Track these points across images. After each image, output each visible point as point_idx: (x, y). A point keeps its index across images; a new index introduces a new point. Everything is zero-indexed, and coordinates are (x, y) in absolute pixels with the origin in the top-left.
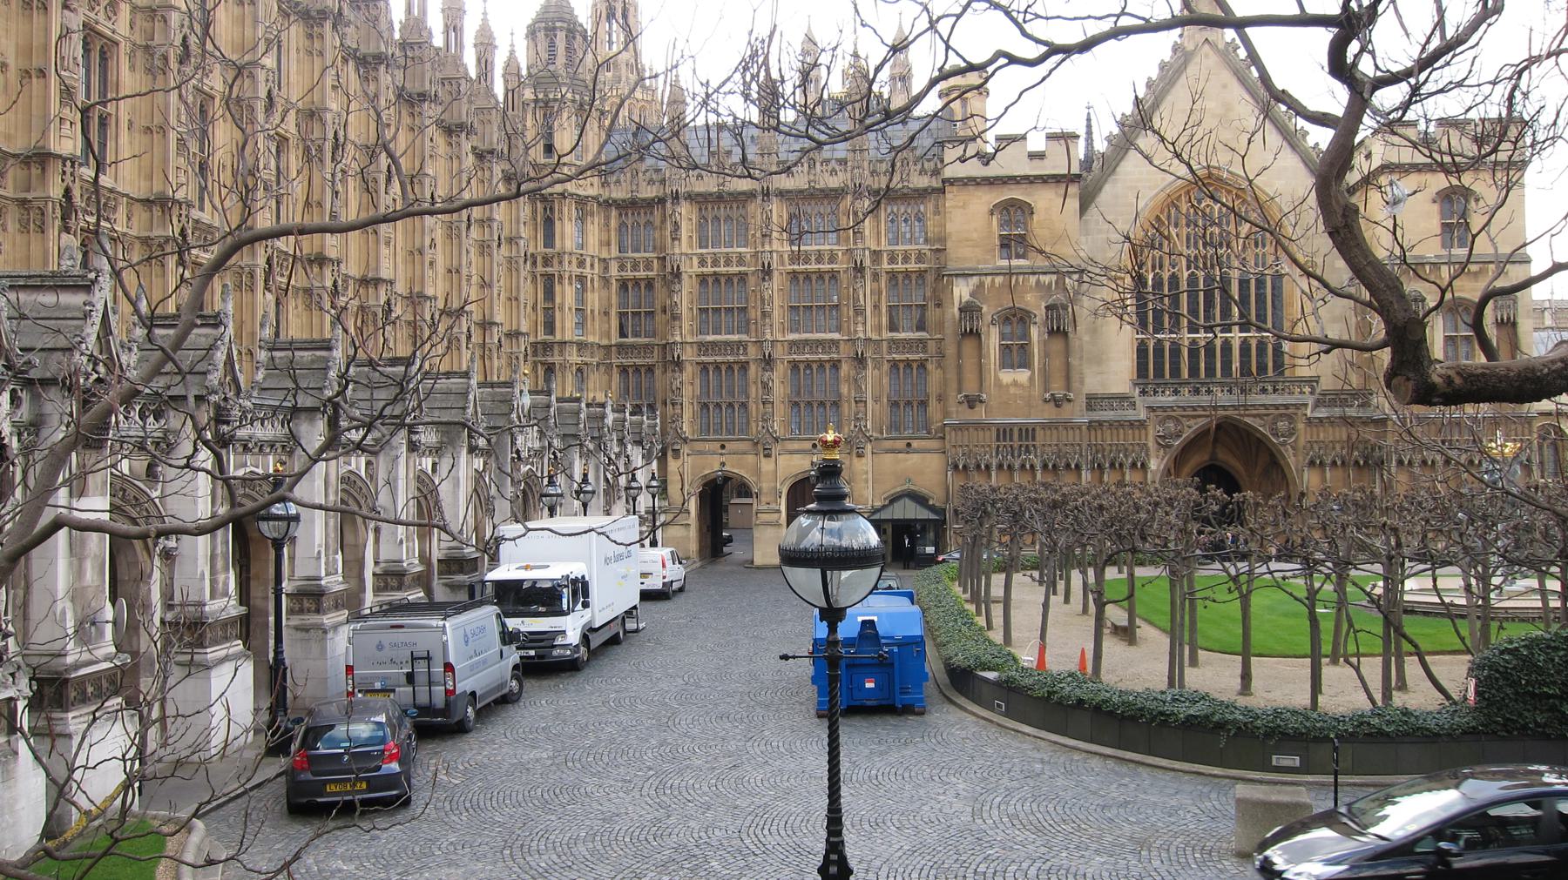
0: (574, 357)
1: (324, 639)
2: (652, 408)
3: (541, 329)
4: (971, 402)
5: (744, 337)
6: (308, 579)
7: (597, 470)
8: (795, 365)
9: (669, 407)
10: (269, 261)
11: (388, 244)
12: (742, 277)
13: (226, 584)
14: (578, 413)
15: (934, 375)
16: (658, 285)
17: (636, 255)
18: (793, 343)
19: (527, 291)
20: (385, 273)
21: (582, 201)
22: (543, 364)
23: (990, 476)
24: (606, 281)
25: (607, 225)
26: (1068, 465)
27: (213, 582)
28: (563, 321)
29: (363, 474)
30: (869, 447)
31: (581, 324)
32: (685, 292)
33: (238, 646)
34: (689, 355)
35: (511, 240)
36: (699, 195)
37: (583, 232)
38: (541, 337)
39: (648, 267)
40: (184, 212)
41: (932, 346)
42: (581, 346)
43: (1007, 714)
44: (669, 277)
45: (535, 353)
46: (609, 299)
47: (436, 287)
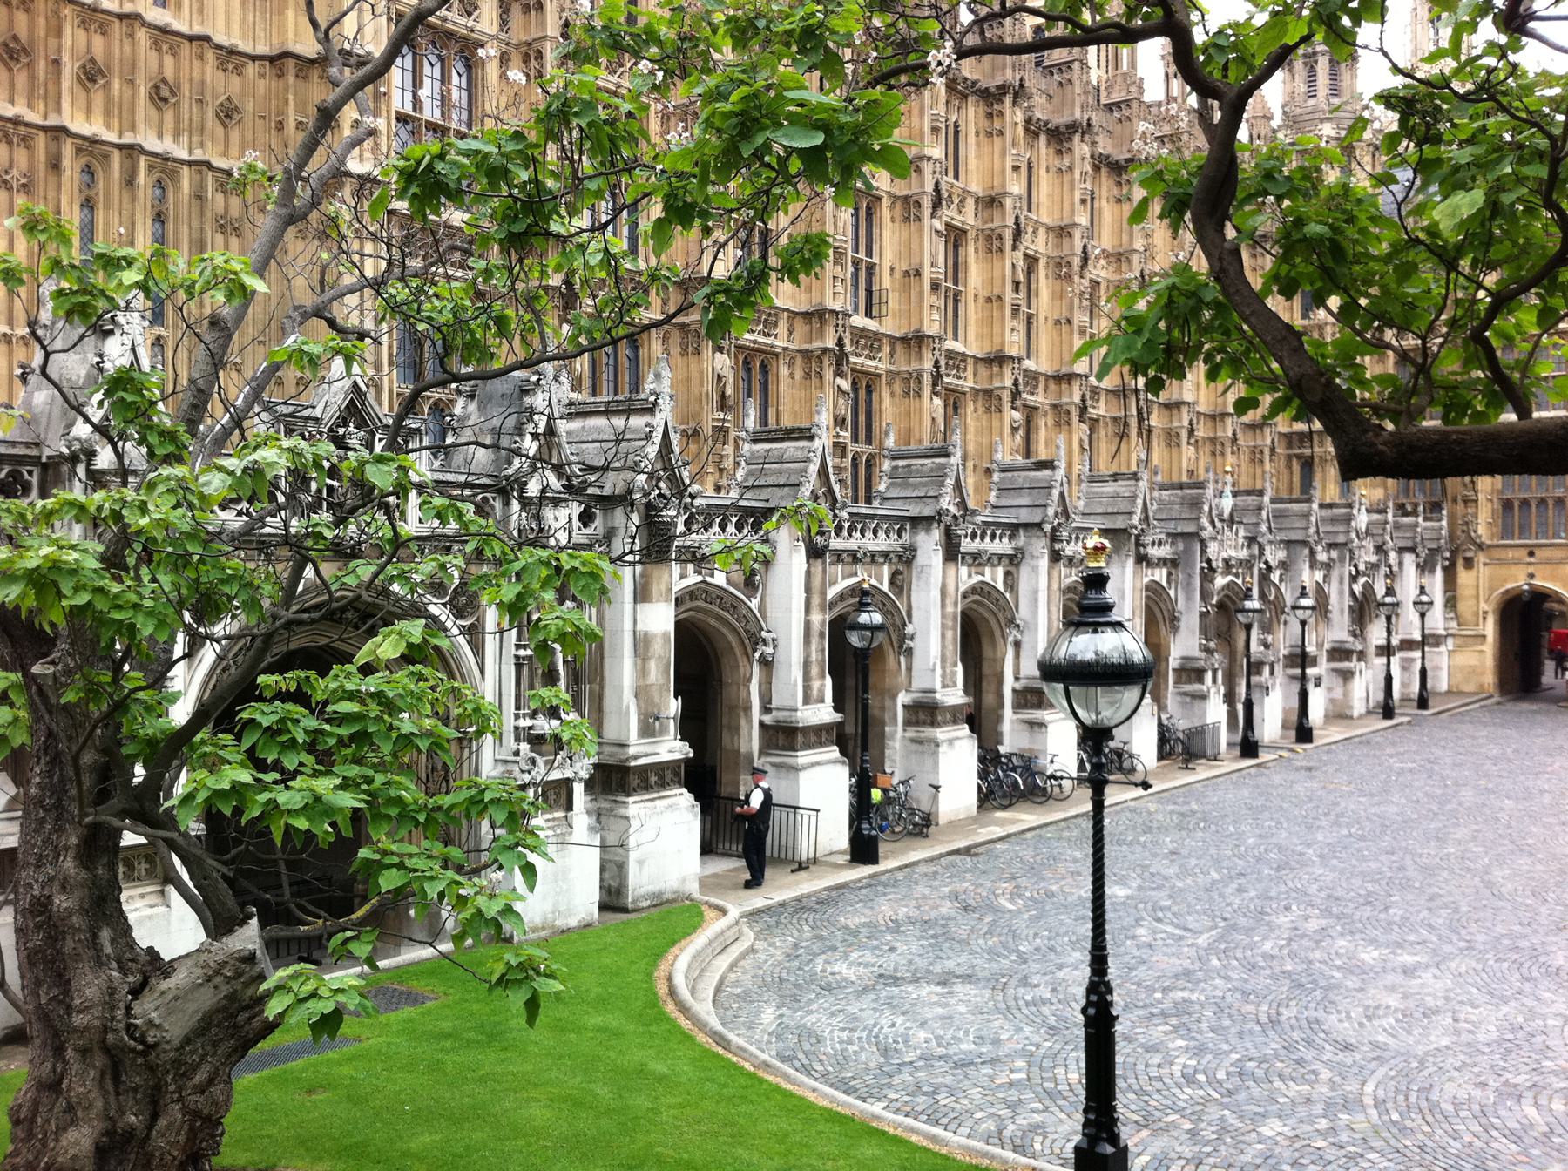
1: (936, 753)
6: (925, 692)
10: (936, 365)
13: (821, 691)
14: (1307, 515)
22: (1299, 457)
29: (1000, 586)
33: (833, 752)
40: (840, 322)
45: (1289, 446)
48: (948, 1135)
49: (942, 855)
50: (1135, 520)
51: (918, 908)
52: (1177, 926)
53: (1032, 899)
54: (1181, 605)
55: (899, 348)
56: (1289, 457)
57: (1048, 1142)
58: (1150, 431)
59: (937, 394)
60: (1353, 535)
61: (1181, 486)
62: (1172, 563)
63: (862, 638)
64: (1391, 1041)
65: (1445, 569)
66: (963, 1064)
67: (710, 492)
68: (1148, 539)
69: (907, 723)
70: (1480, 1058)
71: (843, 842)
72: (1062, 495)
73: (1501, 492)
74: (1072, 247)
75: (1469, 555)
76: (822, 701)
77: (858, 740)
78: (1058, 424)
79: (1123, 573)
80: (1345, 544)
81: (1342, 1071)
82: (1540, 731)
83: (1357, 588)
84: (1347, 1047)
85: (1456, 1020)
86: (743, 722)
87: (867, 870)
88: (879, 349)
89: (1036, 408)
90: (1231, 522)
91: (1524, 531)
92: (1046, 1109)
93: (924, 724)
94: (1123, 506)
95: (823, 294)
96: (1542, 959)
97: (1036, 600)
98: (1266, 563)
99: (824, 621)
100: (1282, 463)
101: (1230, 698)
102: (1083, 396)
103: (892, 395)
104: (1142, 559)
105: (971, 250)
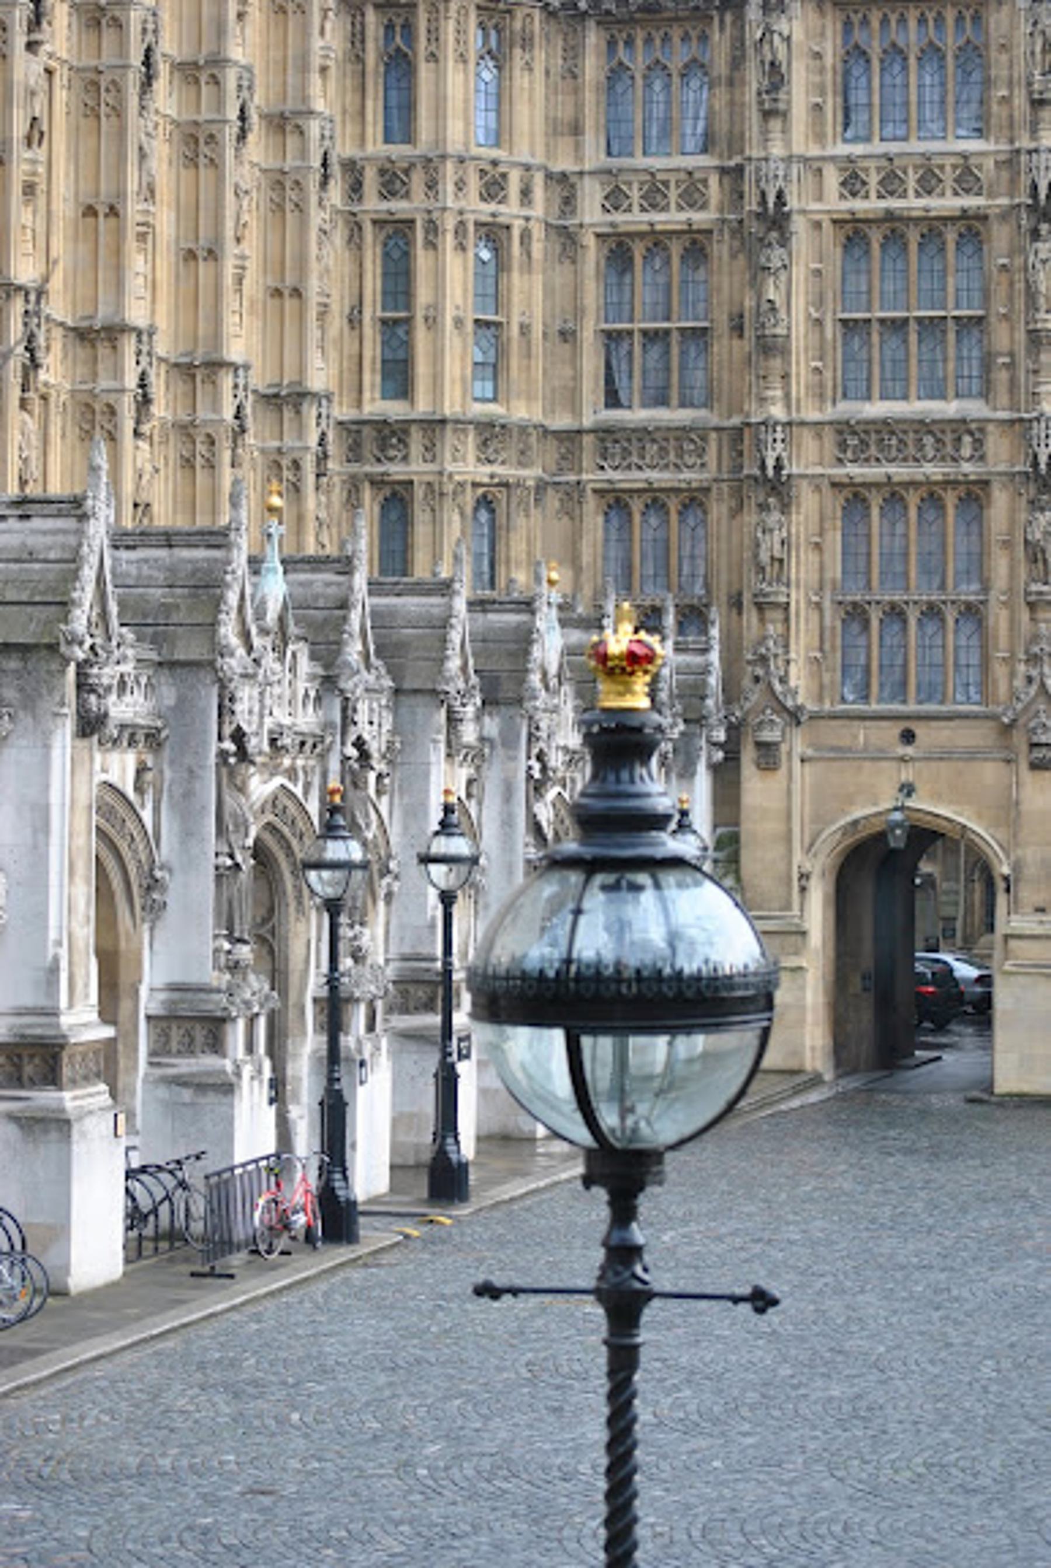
0: (466, 464)
2: (694, 617)
3: (371, 378)
5: (975, 408)
7: (508, 794)
9: (750, 616)
12: (972, 227)
16: (720, 249)
19: (331, 269)
22: (377, 482)
24: (566, 239)
25: (573, 74)
28: (437, 357)
31: (494, 368)
32: (799, 273)
34: (808, 460)
37: (501, 100)
38: (376, 406)
39: (693, 197)
42: (491, 434)
44: (755, 227)
45: (354, 453)
46: (577, 290)
54: (166, 851)
56: (353, 485)
61: (168, 539)
65: (715, 769)
67: (898, 1417)
75: (768, 735)
98: (359, 743)
100: (338, 495)
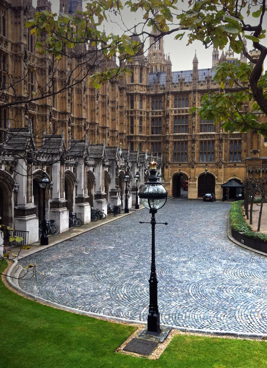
3: (130, 132)
4: (255, 152)
8: (201, 142)
10: (50, 113)
11: (84, 108)
13: (31, 200)
14: (136, 155)
15: (244, 145)
16: (162, 119)
17: (157, 110)
18: (201, 135)
19: (126, 121)
20: (84, 117)
21: (141, 95)
23: (260, 174)
24: (148, 118)
25: (149, 102)
26: (256, 171)
27: (28, 199)
28: (136, 130)
29: (72, 171)
30: (223, 165)
32: (170, 121)
34: (171, 139)
35: (121, 107)
36: (175, 92)
41: (243, 135)
42: (141, 137)
43: (245, 244)
45: (128, 139)
46: (149, 123)
47: (99, 121)
48: (98, 314)
49: (63, 241)
50: (103, 155)
51: (63, 255)
52: (128, 255)
53: (91, 251)
54: (111, 177)
55: (40, 108)
56: (128, 142)
57: (124, 314)
58: (99, 134)
59: (51, 121)
60: (145, 160)
62: (109, 166)
63: (43, 185)
64: (189, 279)
65: (162, 168)
66: (93, 296)
68: (105, 160)
69: (51, 207)
70: (210, 282)
71: (37, 239)
72: (64, 146)
73: (173, 151)
74: (82, 86)
75: (167, 165)
76: (31, 202)
77: (40, 213)
78: (79, 131)
79: (100, 169)
80: (143, 162)
81: (182, 287)
82: (185, 205)
83: (146, 173)
84: (180, 282)
85: (201, 273)
86: (9, 208)
87: (46, 247)
88: (35, 108)
89: (73, 126)
90: (121, 157)
91: (178, 160)
92: (119, 305)
93: (56, 207)
94: (99, 152)
95: (21, 92)
96: (212, 258)
97: (81, 175)
98: (129, 166)
99: (32, 181)
101: (121, 199)
102: (85, 124)
103: (39, 121)
104: (104, 165)
105: (57, 84)
